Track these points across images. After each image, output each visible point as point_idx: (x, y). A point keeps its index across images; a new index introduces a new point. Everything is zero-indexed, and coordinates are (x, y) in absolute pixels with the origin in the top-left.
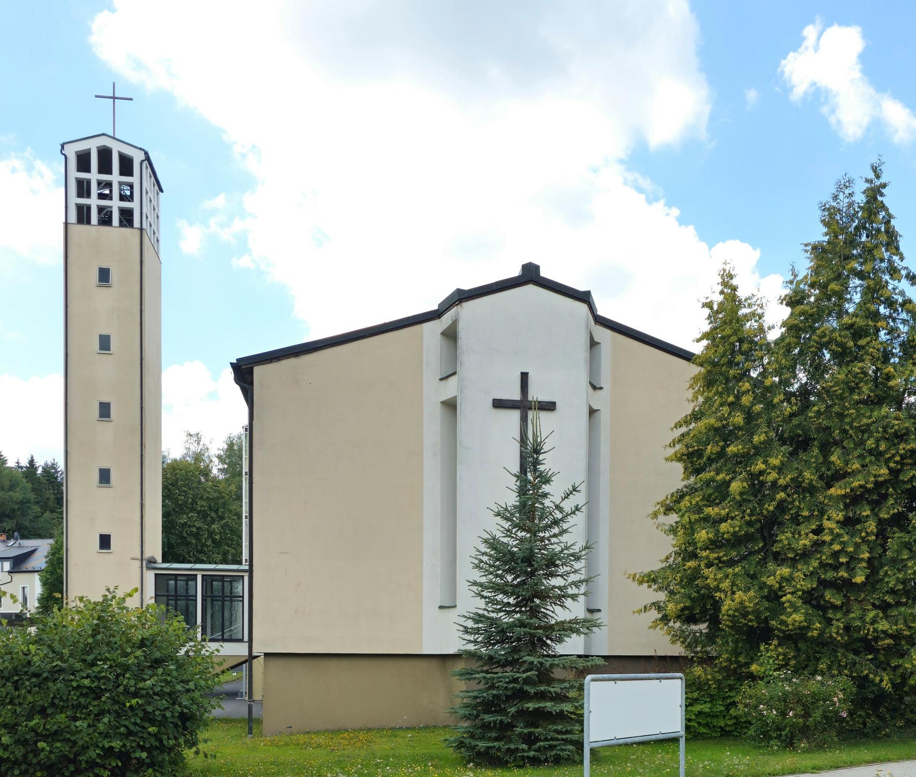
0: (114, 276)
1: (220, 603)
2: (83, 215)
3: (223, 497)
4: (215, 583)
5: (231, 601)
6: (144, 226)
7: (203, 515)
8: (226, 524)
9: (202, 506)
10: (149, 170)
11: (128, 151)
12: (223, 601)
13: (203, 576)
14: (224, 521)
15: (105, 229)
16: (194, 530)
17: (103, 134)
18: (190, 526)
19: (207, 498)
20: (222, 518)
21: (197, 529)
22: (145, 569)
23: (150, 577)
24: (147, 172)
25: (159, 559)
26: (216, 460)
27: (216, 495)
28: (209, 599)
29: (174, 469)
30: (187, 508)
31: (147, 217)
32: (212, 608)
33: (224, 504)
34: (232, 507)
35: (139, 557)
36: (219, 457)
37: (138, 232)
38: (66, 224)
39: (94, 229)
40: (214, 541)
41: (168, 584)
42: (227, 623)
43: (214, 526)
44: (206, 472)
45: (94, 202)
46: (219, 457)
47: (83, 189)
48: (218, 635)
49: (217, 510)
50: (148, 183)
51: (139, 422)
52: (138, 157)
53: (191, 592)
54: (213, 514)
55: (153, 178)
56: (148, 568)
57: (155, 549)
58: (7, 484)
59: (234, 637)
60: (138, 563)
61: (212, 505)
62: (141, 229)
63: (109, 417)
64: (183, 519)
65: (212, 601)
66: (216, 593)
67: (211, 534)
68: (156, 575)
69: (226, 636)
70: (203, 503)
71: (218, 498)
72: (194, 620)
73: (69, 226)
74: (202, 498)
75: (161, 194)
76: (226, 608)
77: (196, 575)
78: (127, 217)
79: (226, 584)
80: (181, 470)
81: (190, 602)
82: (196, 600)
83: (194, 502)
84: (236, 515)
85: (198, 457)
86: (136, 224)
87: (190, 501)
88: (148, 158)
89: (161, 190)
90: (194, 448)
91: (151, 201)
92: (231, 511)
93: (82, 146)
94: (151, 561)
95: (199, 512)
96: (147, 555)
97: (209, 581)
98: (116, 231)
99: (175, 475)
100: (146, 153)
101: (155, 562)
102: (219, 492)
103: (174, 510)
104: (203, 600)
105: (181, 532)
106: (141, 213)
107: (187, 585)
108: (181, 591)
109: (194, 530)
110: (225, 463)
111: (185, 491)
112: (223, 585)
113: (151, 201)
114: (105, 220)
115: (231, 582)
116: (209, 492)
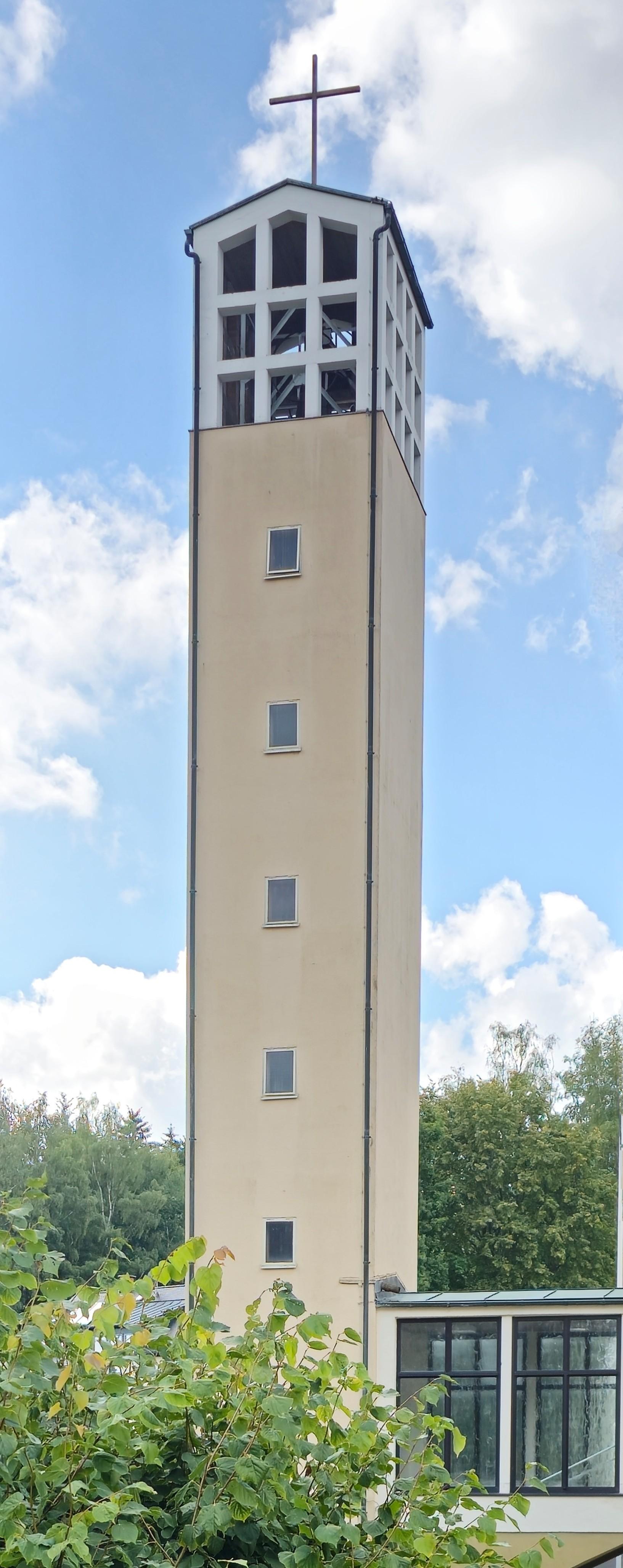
0: (306, 551)
1: (559, 1393)
2: (236, 404)
3: (575, 1160)
4: (546, 1342)
5: (588, 1387)
6: (381, 404)
7: (529, 1204)
8: (580, 1225)
9: (526, 1184)
10: (396, 258)
11: (342, 213)
12: (567, 1388)
13: (516, 1320)
14: (575, 1216)
15: (290, 427)
16: (509, 1239)
17: (287, 183)
18: (498, 1232)
19: (540, 1165)
20: (570, 1209)
21: (515, 1237)
22: (372, 1306)
23: (385, 1328)
24: (390, 267)
25: (410, 1279)
26: (560, 1088)
27: (557, 1155)
28: (532, 1382)
29: (467, 1101)
30: (492, 1188)
31: (389, 384)
32: (539, 1404)
33: (577, 1175)
34: (596, 1183)
35: (360, 1277)
36: (567, 1079)
37: (366, 420)
38: (196, 432)
39: (265, 431)
40: (553, 1264)
41: (430, 1346)
42: (576, 1446)
43: (552, 1230)
44: (537, 1107)
45: (262, 363)
46: (567, 1079)
47: (237, 335)
48: (554, 1476)
49: (560, 1191)
50: (393, 295)
51: (363, 923)
52: (365, 223)
53: (488, 1365)
54: (550, 1201)
55: (406, 285)
56: (382, 1306)
57: (400, 1254)
58: (139, 1173)
59: (592, 1485)
60: (357, 1292)
61: (549, 1179)
62: (374, 412)
63: (292, 916)
64: (485, 1217)
65: (539, 1388)
66: (548, 1367)
67: (546, 1247)
68: (400, 1321)
69: (574, 1480)
70: (528, 1176)
71: (563, 1163)
72: (490, 1438)
73: (204, 437)
74: (525, 1165)
75: (427, 331)
76: (573, 1415)
77: (498, 1319)
78: (339, 384)
79: (574, 1342)
80: (482, 1102)
81: (484, 1393)
82: (497, 1388)
83: (509, 1177)
84: (601, 1200)
85: (519, 1079)
86: (363, 401)
87: (500, 1173)
88: (392, 224)
89: (429, 324)
90: (514, 1062)
91: (399, 344)
92: (590, 1192)
93: (231, 227)
94: (390, 1288)
95: (519, 1198)
96: (378, 1271)
97: (532, 1336)
98: (315, 427)
99: (469, 1116)
100: (389, 210)
101: (397, 1291)
102: (565, 1148)
103: (464, 1197)
104: (515, 1387)
105: (480, 1249)
106: (375, 369)
107: (477, 1347)
108: (461, 1364)
109: (509, 1239)
110: (579, 1091)
111: (488, 1152)
112: (567, 1347)
113: (399, 344)
114: (289, 402)
115: (586, 1335)
116: (542, 1150)
